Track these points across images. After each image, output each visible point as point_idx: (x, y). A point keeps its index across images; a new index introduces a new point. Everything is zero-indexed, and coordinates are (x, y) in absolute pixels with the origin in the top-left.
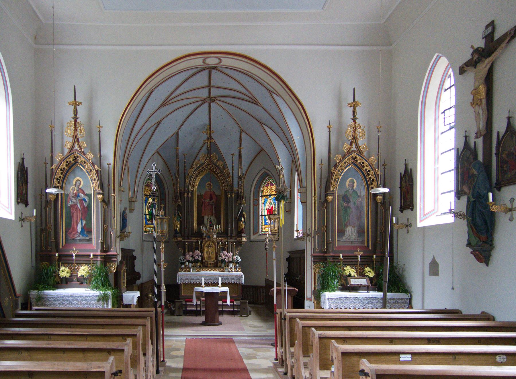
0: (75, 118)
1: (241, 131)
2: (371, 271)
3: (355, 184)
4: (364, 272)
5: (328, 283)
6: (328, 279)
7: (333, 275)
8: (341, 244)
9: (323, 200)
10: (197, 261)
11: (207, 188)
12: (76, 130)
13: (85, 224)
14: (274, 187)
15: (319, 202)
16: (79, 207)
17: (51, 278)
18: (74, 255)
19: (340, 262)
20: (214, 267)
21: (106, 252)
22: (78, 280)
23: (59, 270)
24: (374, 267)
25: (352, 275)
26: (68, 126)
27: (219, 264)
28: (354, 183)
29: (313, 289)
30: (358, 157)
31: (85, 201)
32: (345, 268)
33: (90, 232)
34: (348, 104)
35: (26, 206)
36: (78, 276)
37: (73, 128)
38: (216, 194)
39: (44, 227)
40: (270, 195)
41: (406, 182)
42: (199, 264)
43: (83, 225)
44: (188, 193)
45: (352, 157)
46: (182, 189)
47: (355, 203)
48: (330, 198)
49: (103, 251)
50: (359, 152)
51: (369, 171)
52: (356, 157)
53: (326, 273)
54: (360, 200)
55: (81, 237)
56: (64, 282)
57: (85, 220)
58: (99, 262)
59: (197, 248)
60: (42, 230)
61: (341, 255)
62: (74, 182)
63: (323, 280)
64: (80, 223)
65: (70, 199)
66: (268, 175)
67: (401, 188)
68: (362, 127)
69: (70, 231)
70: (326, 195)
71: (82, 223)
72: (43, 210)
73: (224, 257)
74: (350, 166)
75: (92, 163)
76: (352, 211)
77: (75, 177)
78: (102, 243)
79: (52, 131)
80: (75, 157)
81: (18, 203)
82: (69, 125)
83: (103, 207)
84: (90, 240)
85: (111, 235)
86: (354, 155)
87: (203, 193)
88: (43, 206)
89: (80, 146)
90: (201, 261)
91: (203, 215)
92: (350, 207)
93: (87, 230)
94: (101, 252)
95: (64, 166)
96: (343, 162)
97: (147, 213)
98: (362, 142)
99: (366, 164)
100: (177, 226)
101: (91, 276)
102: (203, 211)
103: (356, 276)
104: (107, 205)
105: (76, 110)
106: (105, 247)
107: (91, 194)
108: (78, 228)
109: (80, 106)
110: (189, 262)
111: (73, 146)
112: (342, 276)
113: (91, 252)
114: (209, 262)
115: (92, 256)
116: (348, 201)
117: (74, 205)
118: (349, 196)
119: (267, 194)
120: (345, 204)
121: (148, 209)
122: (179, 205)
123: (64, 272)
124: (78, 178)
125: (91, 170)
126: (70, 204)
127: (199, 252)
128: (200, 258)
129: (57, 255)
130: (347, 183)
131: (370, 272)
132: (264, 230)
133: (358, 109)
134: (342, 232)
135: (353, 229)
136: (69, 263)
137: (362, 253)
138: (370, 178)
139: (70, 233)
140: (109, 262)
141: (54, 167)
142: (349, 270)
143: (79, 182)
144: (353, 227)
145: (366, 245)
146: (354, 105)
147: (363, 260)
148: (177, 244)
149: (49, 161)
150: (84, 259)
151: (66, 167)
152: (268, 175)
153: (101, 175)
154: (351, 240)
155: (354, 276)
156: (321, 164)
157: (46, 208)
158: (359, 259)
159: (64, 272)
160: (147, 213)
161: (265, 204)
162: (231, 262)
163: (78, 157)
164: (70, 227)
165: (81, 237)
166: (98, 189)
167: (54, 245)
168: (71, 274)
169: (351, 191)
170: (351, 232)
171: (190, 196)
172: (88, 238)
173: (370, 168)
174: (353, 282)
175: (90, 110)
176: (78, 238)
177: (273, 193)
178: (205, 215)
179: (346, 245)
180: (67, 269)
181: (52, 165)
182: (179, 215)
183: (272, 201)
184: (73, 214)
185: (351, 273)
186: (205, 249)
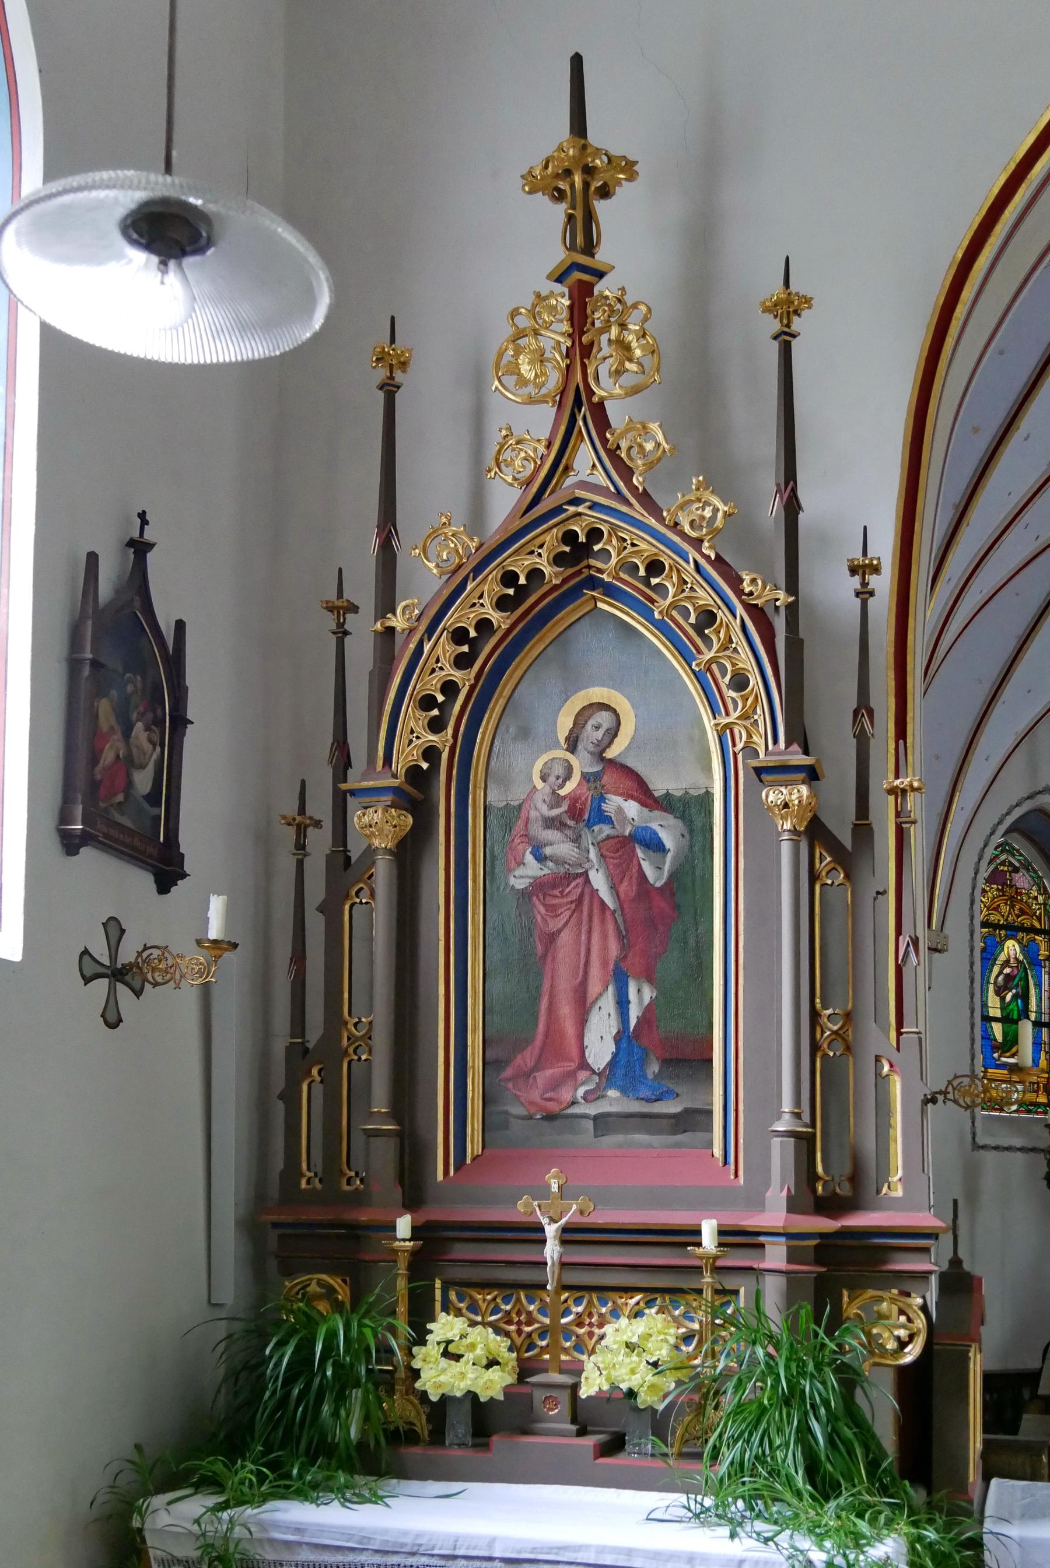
0: (581, 279)
12: (581, 350)
13: (645, 1019)
16: (605, 894)
17: (341, 1398)
18: (551, 1231)
21: (829, 1205)
22: (583, 1417)
23: (420, 1337)
26: (520, 334)
31: (656, 846)
33: (690, 1060)
35: (164, 885)
36: (584, 1393)
37: (556, 335)
39: (314, 1035)
43: (634, 1013)
49: (811, 1195)
55: (614, 1101)
56: (459, 1426)
57: (649, 976)
58: (773, 1289)
60: (300, 1056)
62: (565, 723)
64: (608, 1002)
65: (527, 836)
69: (527, 1058)
71: (622, 1004)
72: (316, 924)
75: (719, 562)
77: (572, 685)
78: (804, 1143)
79: (390, 390)
80: (570, 537)
81: (71, 844)
82: (523, 322)
83: (813, 877)
84: (695, 1120)
85: (882, 1083)
88: (316, 891)
89: (613, 453)
93: (672, 1050)
94: (793, 1206)
95: (481, 604)
97: (995, 1012)
101: (704, 1393)
104: (844, 859)
105: (583, 232)
106: (830, 1176)
107: (707, 797)
108: (591, 1038)
109: (624, 192)
111: (560, 465)
113: (706, 1204)
115: (709, 1240)
117: (566, 880)
121: (999, 992)
123: (460, 1357)
124: (597, 693)
125: (708, 618)
126: (528, 871)
129: (404, 1226)
136: (509, 1288)
139: (526, 1075)
140: (856, 1286)
141: (398, 622)
143: (604, 719)
149: (363, 590)
150: (648, 1261)
151: (495, 617)
153: (795, 645)
157: (331, 909)
159: (460, 1357)
160: (995, 1012)
163: (595, 534)
164: (524, 1037)
165: (614, 1101)
166: (768, 744)
167: (383, 1158)
168: (525, 1371)
172: (671, 1107)
175: (701, 241)
176: (592, 1110)
180: (484, 1340)
181: (386, 604)
184: (551, 938)
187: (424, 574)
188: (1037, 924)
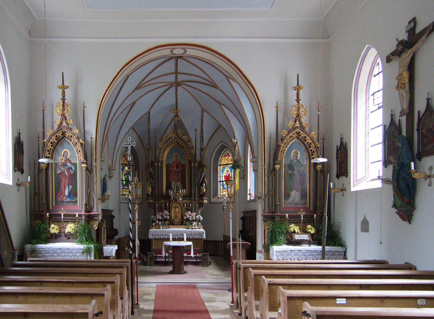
0: (63, 100)
1: (203, 110)
2: (312, 228)
3: (299, 155)
4: (306, 229)
5: (276, 239)
6: (276, 235)
7: (280, 232)
8: (287, 205)
9: (271, 168)
10: (166, 220)
11: (174, 158)
12: (64, 110)
13: (71, 189)
14: (230, 158)
15: (269, 170)
16: (67, 175)
17: (42, 234)
18: (62, 215)
19: (286, 220)
20: (180, 225)
21: (89, 212)
22: (66, 235)
23: (50, 227)
24: (315, 224)
25: (296, 232)
26: (57, 106)
27: (184, 222)
28: (298, 154)
29: (263, 244)
30: (301, 132)
31: (72, 169)
32: (291, 226)
33: (75, 195)
34: (293, 88)
35: (22, 173)
36: (66, 232)
37: (61, 108)
38: (182, 163)
39: (37, 191)
40: (227, 165)
41: (341, 153)
42: (167, 222)
43: (70, 189)
44: (158, 162)
45: (296, 132)
46: (153, 159)
47: (298, 171)
48: (277, 166)
49: (87, 211)
50: (302, 128)
51: (310, 144)
52: (299, 133)
53: (274, 230)
54: (303, 168)
55: (68, 199)
56: (54, 237)
57: (71, 185)
58: (83, 221)
59: (166, 209)
60: (35, 194)
61: (287, 215)
62: (62, 153)
63: (272, 236)
64: (67, 188)
65: (59, 167)
66: (225, 147)
67: (337, 158)
68: (305, 107)
69: (59, 194)
70: (274, 164)
71: (69, 188)
72: (37, 177)
73: (188, 216)
74: (294, 140)
75: (78, 137)
76: (296, 178)
77: (63, 149)
78: (86, 205)
79: (43, 111)
80: (63, 132)
81: (15, 171)
82: (58, 105)
83: (87, 174)
84: (76, 202)
85: (93, 198)
86: (298, 130)
87: (170, 163)
88: (36, 174)
89: (67, 123)
90: (169, 220)
91: (170, 181)
92: (294, 174)
93: (73, 194)
94: (85, 212)
95: (54, 139)
96: (289, 136)
97: (124, 179)
98: (304, 120)
99: (308, 138)
100: (149, 191)
101: (76, 232)
102: (171, 177)
103: (299, 232)
104: (90, 172)
105: (64, 93)
106: (89, 208)
107: (77, 164)
108: (66, 192)
109: (67, 89)
110: (159, 220)
111: (61, 123)
112: (287, 232)
113: (77, 212)
114: (176, 221)
115: (77, 216)
116: (293, 170)
117: (63, 173)
118: (293, 165)
119: (224, 163)
120: (290, 171)
121: (125, 176)
122: (150, 173)
123: (54, 229)
124: (66, 150)
125: (76, 144)
126: (59, 172)
127: (168, 212)
128: (168, 218)
129: (48, 214)
130: (292, 154)
131: (311, 229)
132: (222, 194)
133: (301, 92)
134: (287, 196)
135: (297, 193)
136: (58, 222)
137: (304, 213)
138: (311, 150)
139: (59, 196)
140: (91, 221)
141: (45, 141)
142: (293, 227)
143: (66, 153)
144: (297, 191)
145: (308, 206)
146: (298, 88)
147: (305, 219)
148: (149, 206)
149: (41, 135)
150: (70, 218)
151: (55, 141)
152: (225, 147)
153: (85, 148)
154: (295, 202)
155: (298, 233)
156: (270, 138)
157: (38, 175)
158: (302, 218)
159: (54, 229)
160: (124, 179)
161: (223, 171)
162: (194, 221)
163: (65, 132)
164: (59, 191)
165: (68, 199)
166: (82, 159)
167: (45, 206)
168: (60, 231)
169: (295, 161)
170: (295, 195)
171: (160, 165)
172: (74, 200)
173: (311, 142)
174: (297, 237)
175: (76, 92)
176: (66, 200)
177: (230, 163)
178: (173, 181)
179: (291, 206)
180: (56, 227)
181: (44, 139)
182: (151, 181)
183: (229, 170)
184: (61, 180)
185: (295, 230)
186: (173, 210)
187: (48, 133)
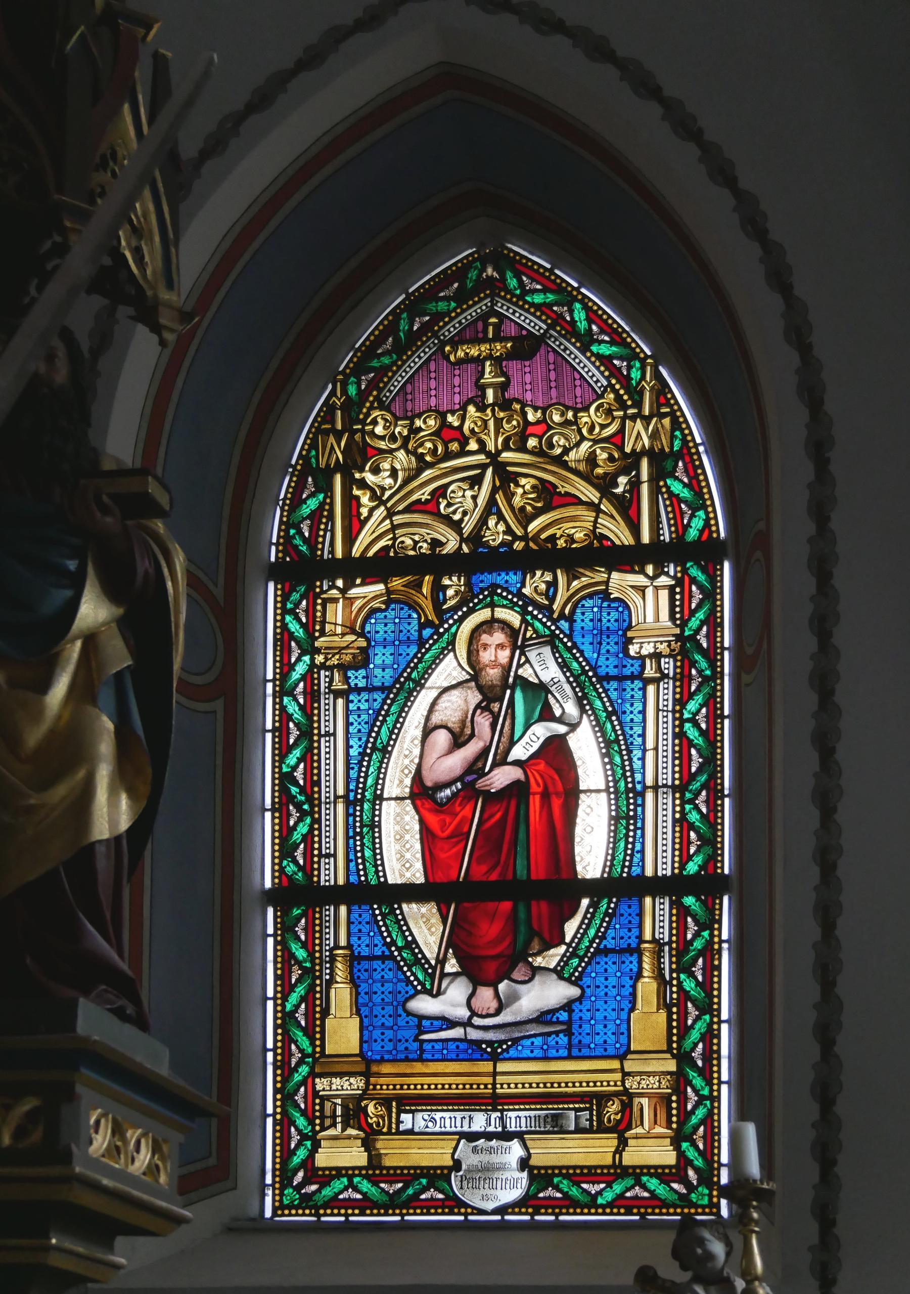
40: (478, 559)
183: (543, 666)
188: (618, 533)
